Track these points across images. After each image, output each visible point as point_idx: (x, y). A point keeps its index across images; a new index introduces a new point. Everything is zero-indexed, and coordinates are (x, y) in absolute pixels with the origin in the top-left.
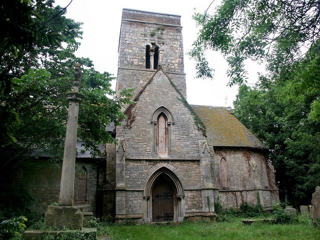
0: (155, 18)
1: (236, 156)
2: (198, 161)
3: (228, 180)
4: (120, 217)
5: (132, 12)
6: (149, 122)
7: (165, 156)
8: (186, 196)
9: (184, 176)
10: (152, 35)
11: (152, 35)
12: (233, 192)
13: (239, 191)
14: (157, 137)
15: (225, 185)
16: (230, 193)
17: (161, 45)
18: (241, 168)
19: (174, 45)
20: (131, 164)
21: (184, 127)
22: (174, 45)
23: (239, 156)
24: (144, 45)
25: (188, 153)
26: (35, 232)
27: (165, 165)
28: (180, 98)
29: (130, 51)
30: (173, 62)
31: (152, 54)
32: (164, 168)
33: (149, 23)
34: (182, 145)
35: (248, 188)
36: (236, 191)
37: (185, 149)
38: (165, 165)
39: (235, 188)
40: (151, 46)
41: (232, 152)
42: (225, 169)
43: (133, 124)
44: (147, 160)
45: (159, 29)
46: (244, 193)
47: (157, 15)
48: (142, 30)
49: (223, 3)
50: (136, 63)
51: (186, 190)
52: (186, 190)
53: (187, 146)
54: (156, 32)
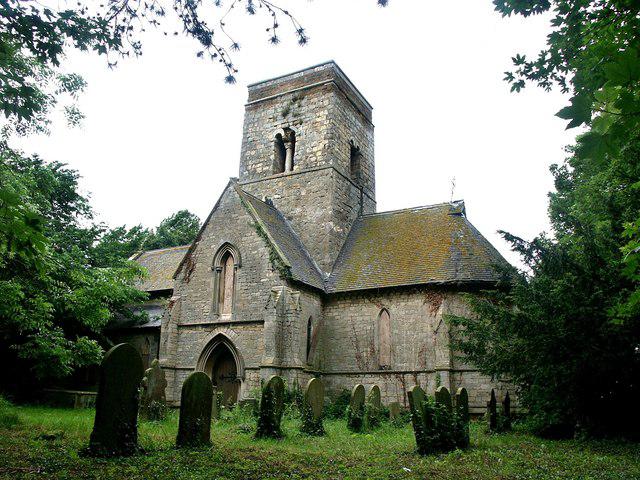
0: (291, 82)
1: (410, 303)
2: (262, 322)
3: (392, 351)
4: (476, 411)
5: (259, 87)
6: (210, 269)
7: (226, 317)
8: (248, 377)
9: (248, 346)
10: (285, 114)
11: (285, 114)
12: (397, 373)
13: (411, 372)
14: (222, 290)
15: (385, 360)
16: (393, 376)
17: (298, 126)
18: (419, 326)
19: (318, 120)
20: (186, 332)
21: (256, 267)
22: (318, 120)
23: (418, 302)
24: (272, 137)
25: (256, 309)
26: (58, 421)
27: (222, 331)
28: (253, 223)
29: (253, 153)
30: (315, 149)
31: (287, 145)
32: (220, 335)
33: (281, 96)
34: (250, 298)
35: (430, 366)
36: (405, 373)
37: (253, 304)
38: (222, 331)
39: (403, 367)
40: (283, 134)
41: (402, 297)
42: (387, 328)
43: (192, 275)
44: (203, 326)
45: (295, 100)
46: (420, 377)
47: (296, 76)
48: (271, 111)
49: (73, 84)
50: (259, 170)
51: (248, 369)
52: (248, 369)
53: (255, 299)
54: (291, 107)
